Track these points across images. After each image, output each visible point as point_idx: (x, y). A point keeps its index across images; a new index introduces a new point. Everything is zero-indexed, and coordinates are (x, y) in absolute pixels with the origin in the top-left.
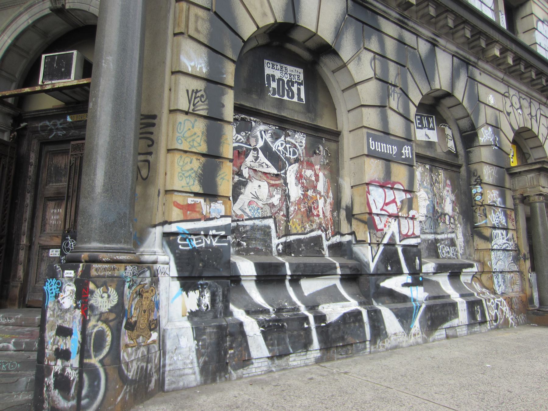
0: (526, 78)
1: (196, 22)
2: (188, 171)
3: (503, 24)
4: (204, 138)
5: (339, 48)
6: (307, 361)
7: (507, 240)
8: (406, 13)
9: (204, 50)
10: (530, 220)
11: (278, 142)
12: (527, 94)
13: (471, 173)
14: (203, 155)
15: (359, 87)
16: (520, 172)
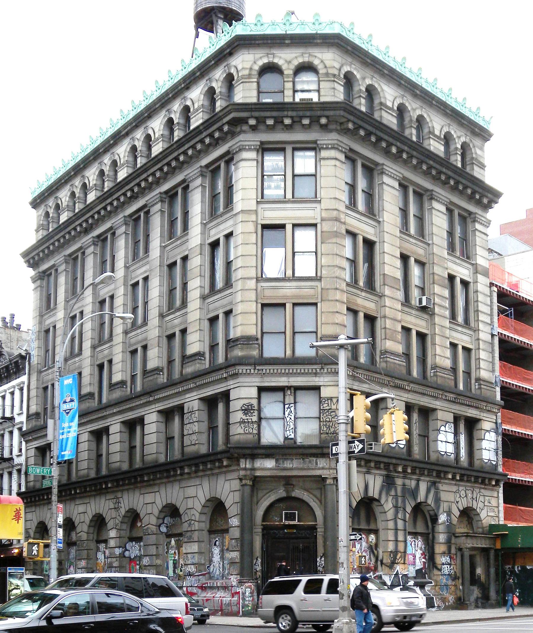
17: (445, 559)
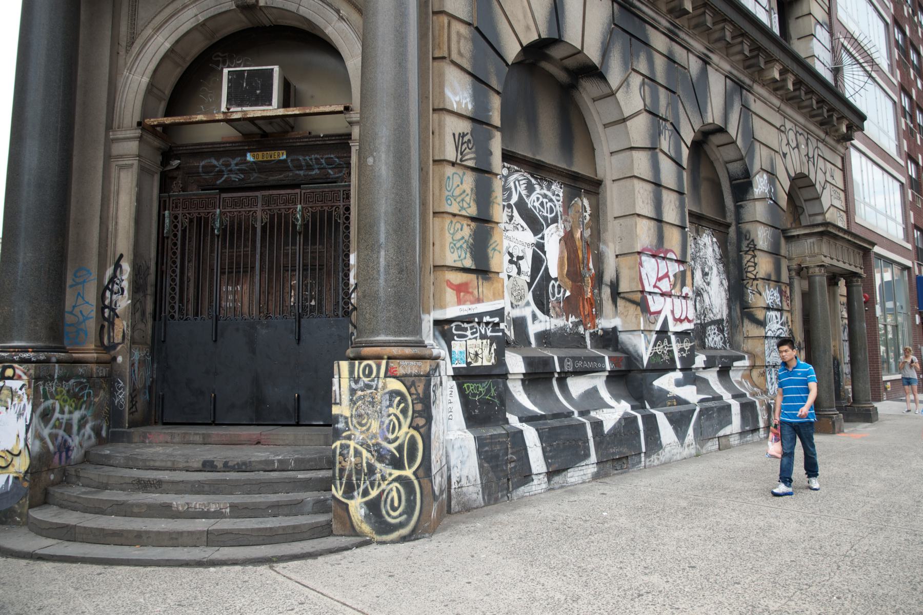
0: (806, 107)
1: (459, 42)
2: (459, 240)
3: (776, 30)
4: (474, 196)
5: (607, 70)
6: (584, 477)
7: (782, 324)
8: (677, 21)
9: (468, 79)
10: (808, 297)
11: (534, 196)
12: (804, 128)
13: (742, 235)
14: (473, 219)
15: (628, 123)
16: (798, 236)
17: (770, 296)
